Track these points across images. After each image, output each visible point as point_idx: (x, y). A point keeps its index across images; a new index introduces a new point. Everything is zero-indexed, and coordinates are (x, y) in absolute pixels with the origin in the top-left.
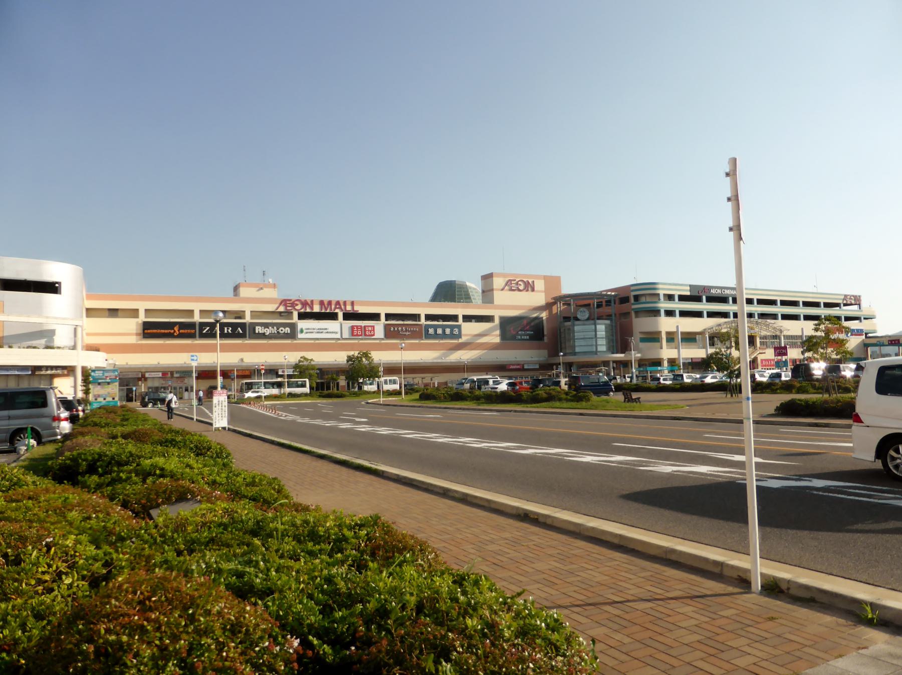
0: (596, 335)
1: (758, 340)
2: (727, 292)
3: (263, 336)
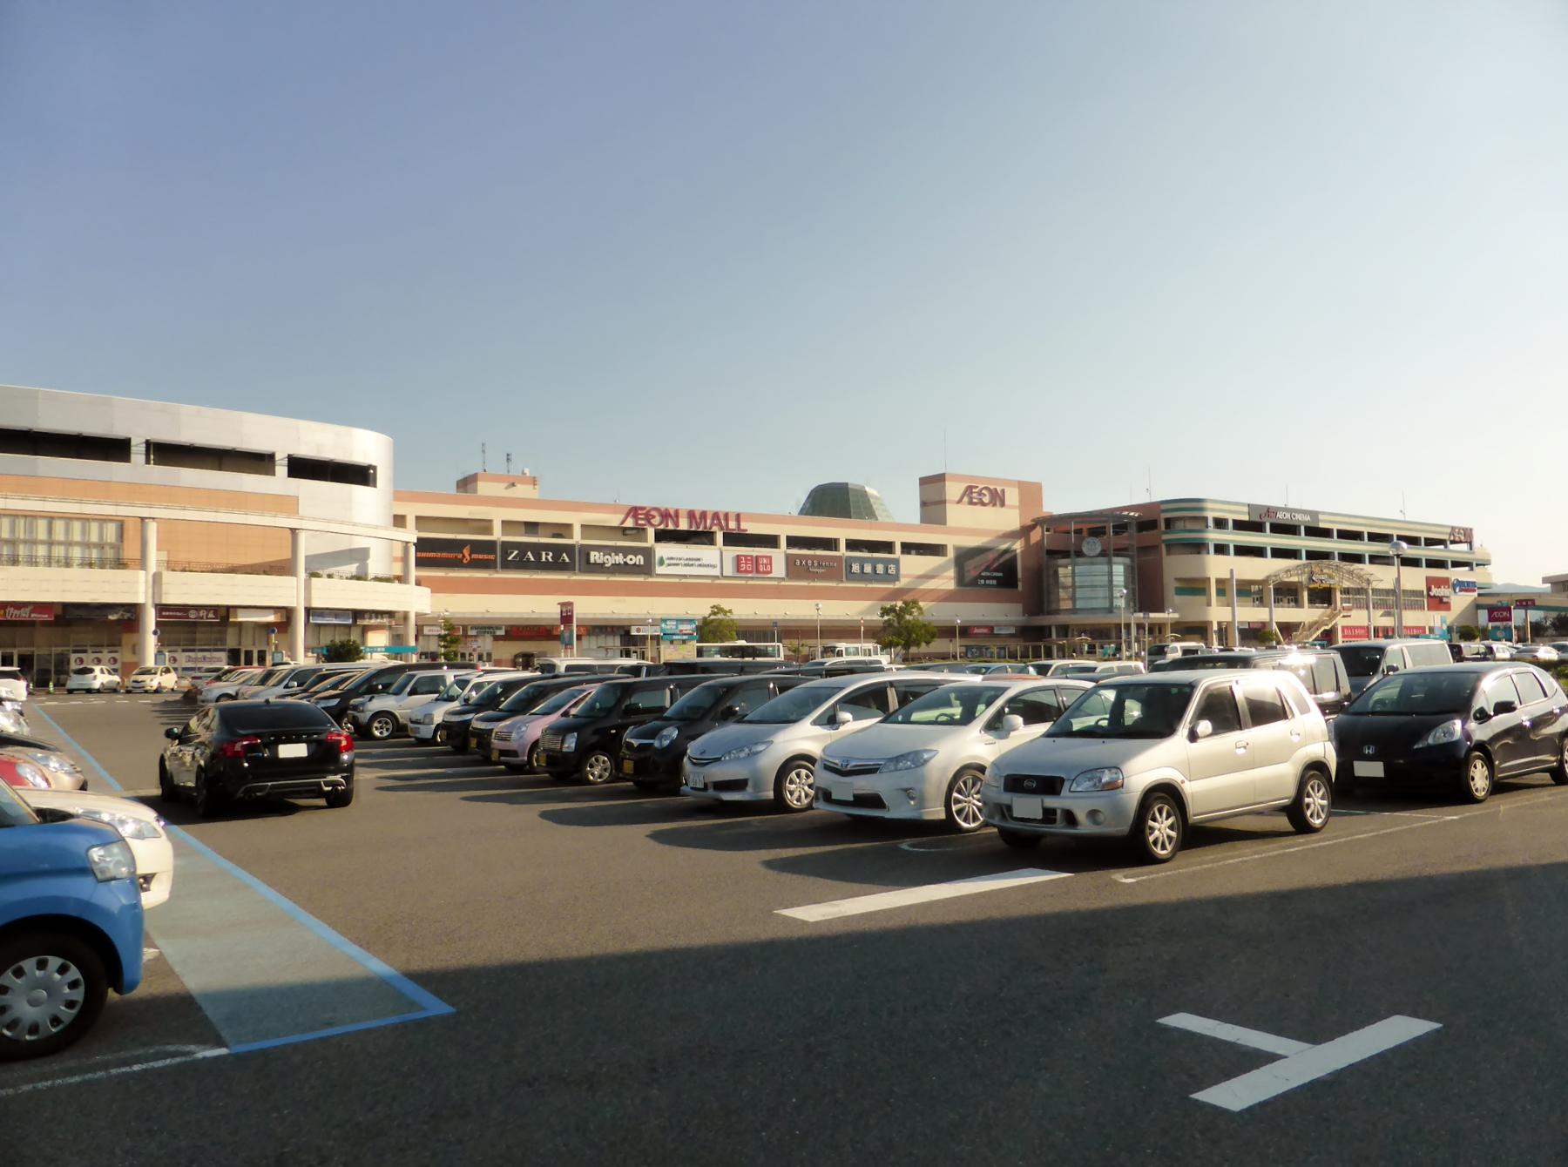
0: (1111, 581)
1: (1338, 595)
2: (1299, 517)
3: (600, 568)
